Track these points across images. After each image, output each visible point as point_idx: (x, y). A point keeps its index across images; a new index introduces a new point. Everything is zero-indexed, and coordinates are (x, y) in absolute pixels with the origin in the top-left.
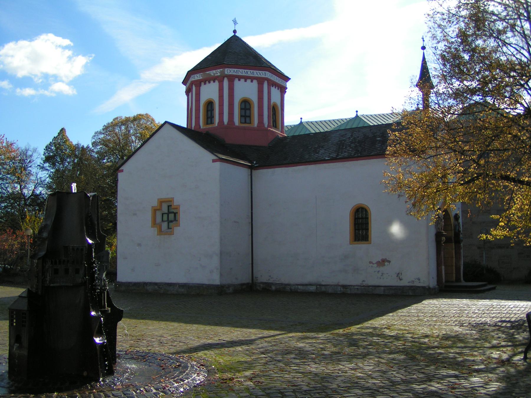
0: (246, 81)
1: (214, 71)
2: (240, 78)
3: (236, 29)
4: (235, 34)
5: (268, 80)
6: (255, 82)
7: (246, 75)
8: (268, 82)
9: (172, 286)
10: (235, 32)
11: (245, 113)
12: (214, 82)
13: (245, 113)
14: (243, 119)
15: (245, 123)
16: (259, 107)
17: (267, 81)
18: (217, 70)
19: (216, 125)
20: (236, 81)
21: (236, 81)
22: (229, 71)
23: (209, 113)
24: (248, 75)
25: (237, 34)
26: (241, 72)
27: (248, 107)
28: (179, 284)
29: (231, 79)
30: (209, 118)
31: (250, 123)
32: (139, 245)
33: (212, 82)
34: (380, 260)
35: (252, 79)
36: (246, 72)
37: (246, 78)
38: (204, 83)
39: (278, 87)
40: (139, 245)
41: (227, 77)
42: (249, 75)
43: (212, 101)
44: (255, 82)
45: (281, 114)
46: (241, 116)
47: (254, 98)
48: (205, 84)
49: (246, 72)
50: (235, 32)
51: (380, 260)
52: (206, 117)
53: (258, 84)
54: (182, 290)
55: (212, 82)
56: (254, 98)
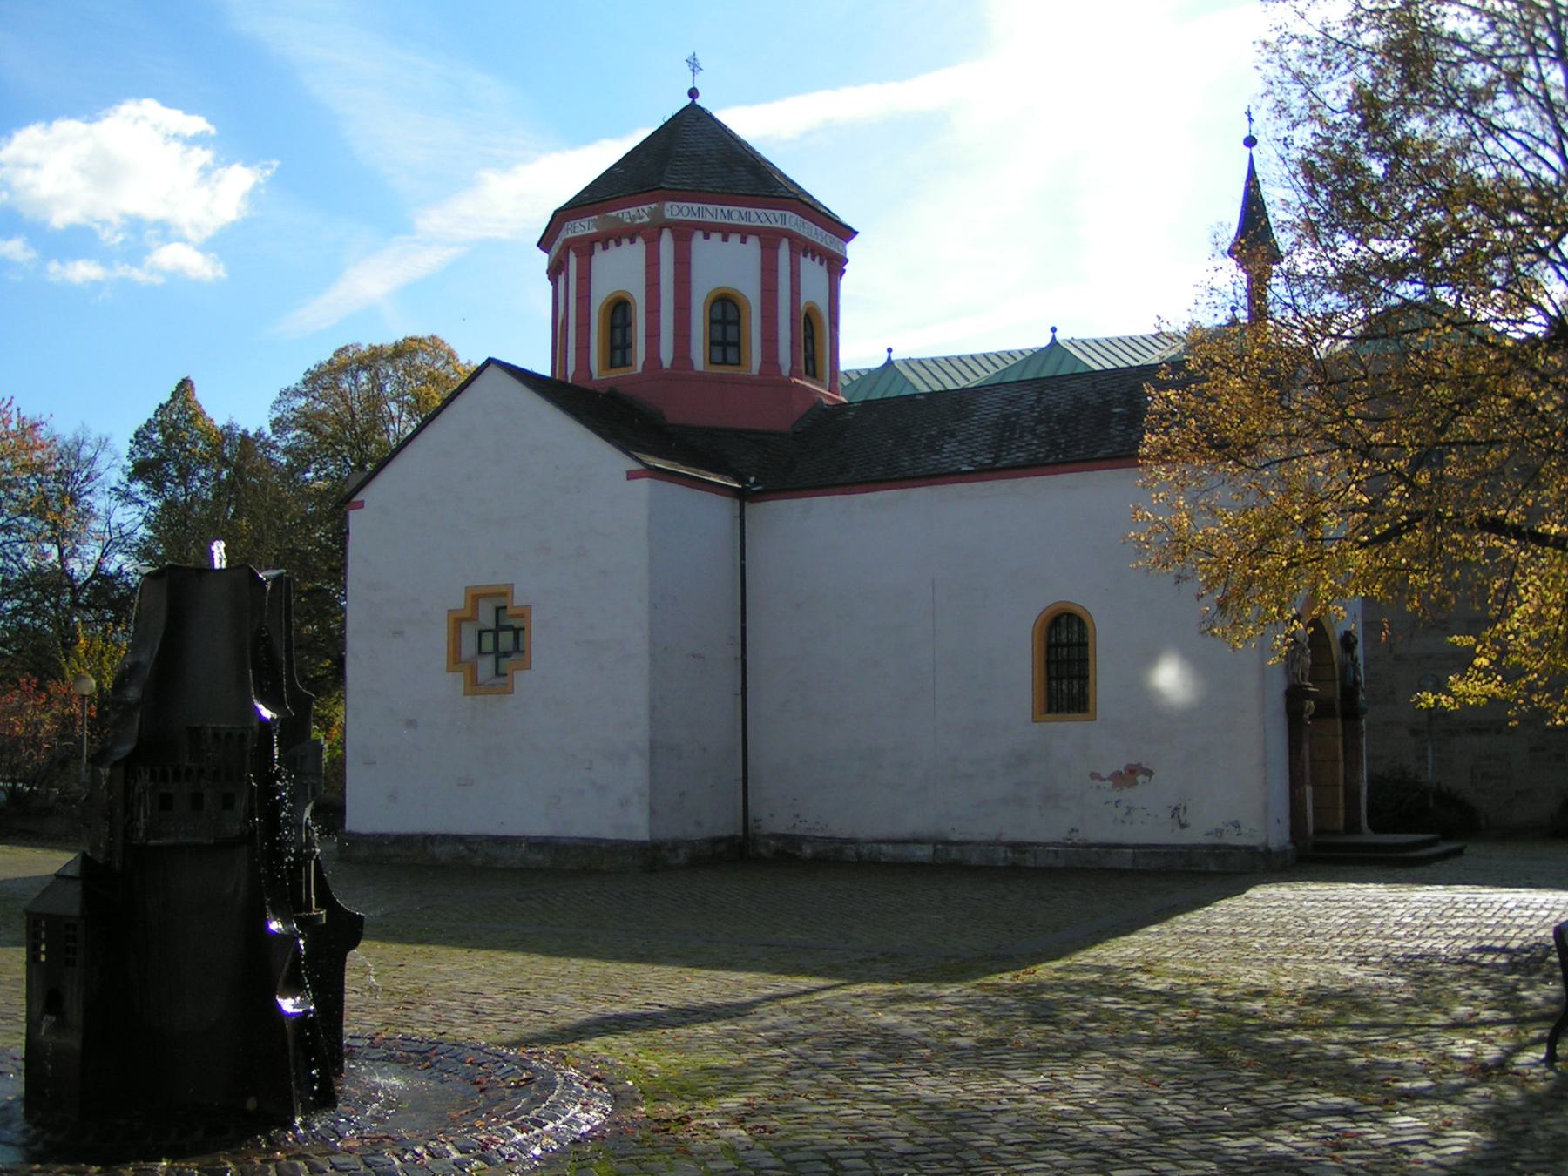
0: (727, 241)
1: (633, 211)
2: (708, 229)
3: (696, 86)
4: (693, 101)
5: (793, 237)
6: (753, 241)
7: (726, 221)
8: (791, 243)
9: (508, 846)
10: (693, 93)
11: (724, 333)
12: (632, 241)
13: (724, 333)
14: (718, 353)
15: (725, 362)
16: (764, 317)
17: (790, 239)
18: (640, 208)
19: (639, 369)
20: (698, 240)
21: (698, 240)
22: (676, 211)
23: (618, 333)
24: (731, 222)
25: (698, 102)
26: (713, 213)
27: (731, 316)
28: (527, 839)
29: (684, 233)
30: (618, 348)
31: (739, 364)
32: (412, 723)
33: (625, 242)
34: (1122, 769)
35: (745, 233)
36: (726, 212)
37: (726, 231)
38: (603, 244)
39: (821, 256)
40: (412, 723)
41: (670, 228)
42: (736, 222)
43: (627, 297)
44: (753, 241)
45: (831, 338)
46: (713, 343)
47: (750, 289)
48: (605, 248)
49: (726, 212)
50: (693, 93)
51: (1122, 769)
52: (608, 345)
53: (762, 248)
54: (538, 857)
55: (625, 242)
56: (750, 289)
